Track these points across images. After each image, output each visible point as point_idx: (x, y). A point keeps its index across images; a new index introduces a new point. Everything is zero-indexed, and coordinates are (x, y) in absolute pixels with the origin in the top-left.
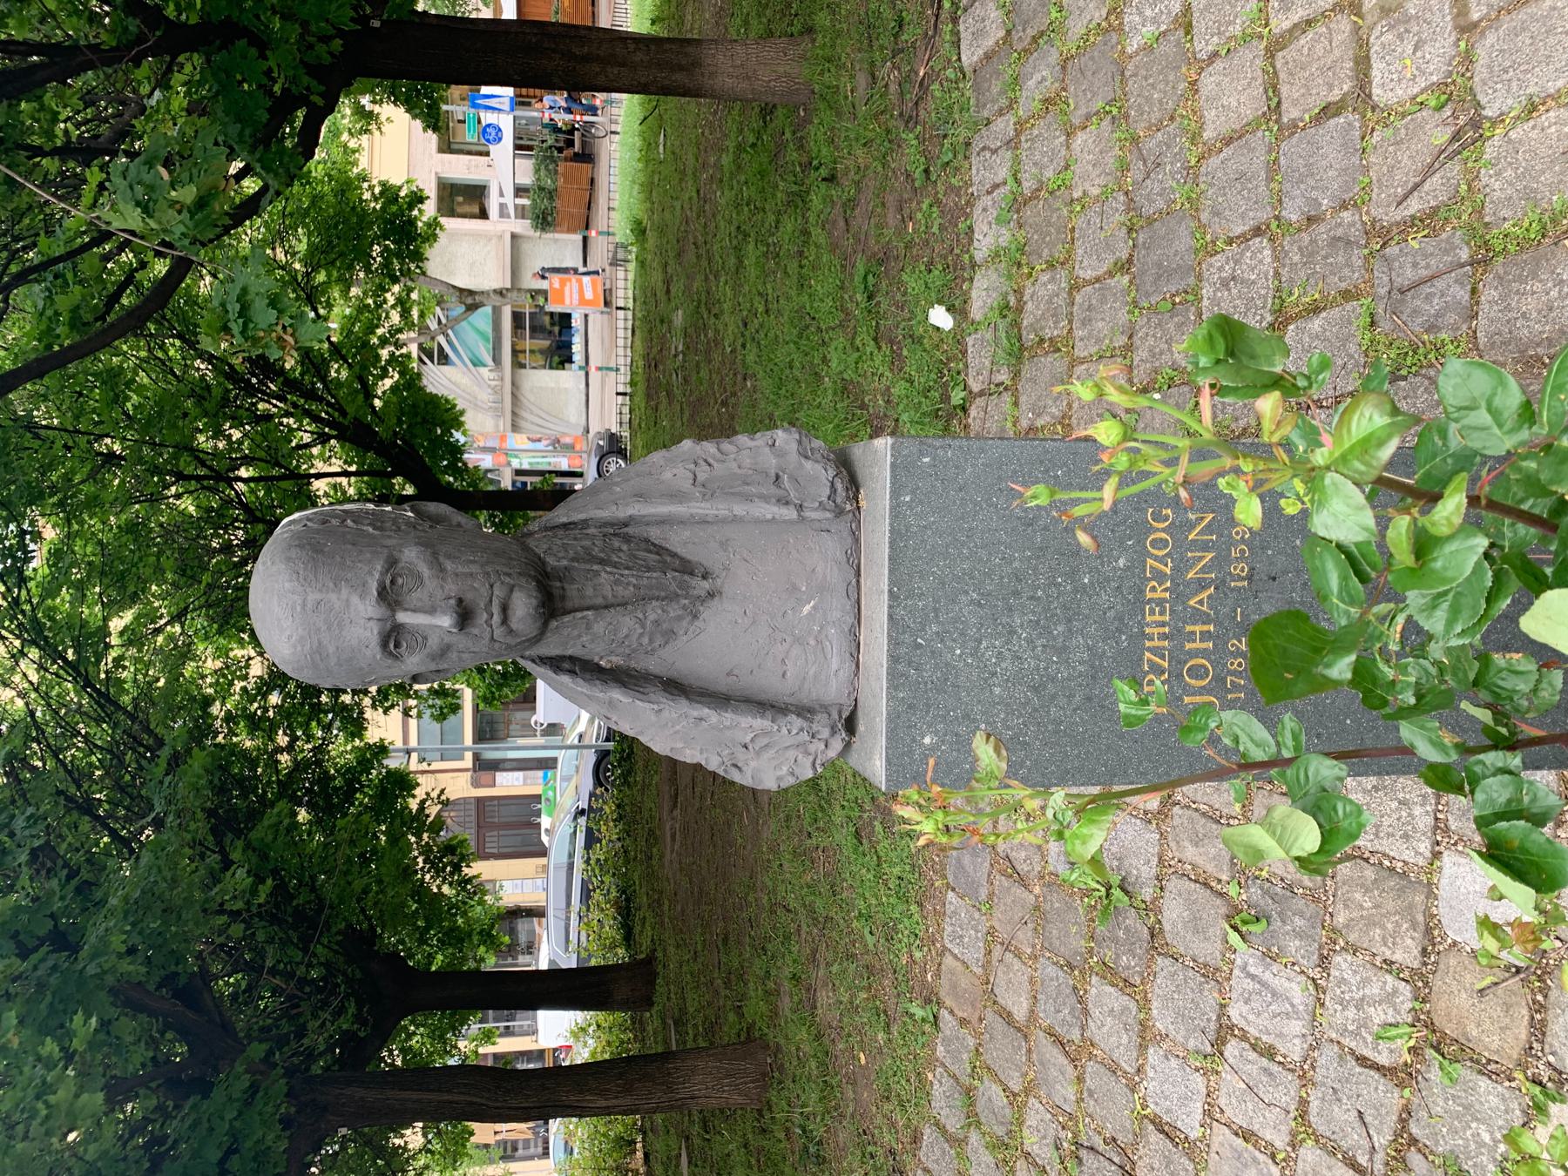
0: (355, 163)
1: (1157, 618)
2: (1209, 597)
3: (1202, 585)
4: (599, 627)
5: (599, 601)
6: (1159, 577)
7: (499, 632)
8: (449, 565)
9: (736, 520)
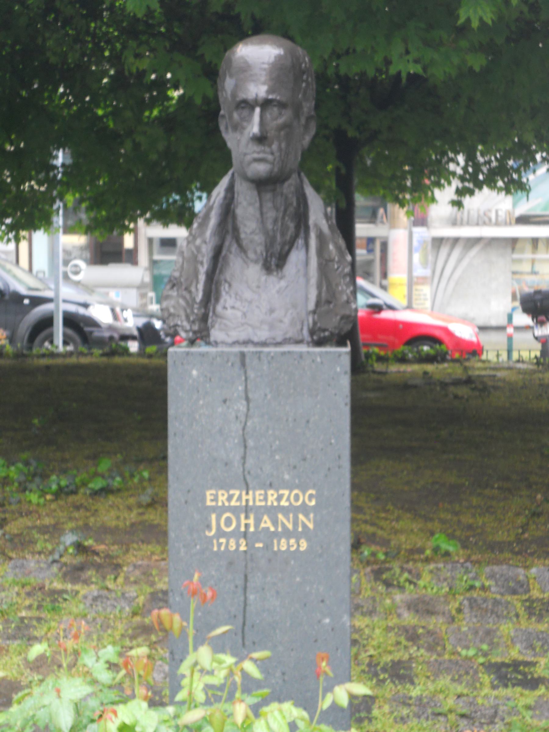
0: (407, 213)
1: (257, 498)
2: (268, 528)
3: (275, 522)
4: (251, 210)
5: (265, 210)
6: (279, 498)
7: (249, 158)
8: (282, 133)
9: (308, 281)
